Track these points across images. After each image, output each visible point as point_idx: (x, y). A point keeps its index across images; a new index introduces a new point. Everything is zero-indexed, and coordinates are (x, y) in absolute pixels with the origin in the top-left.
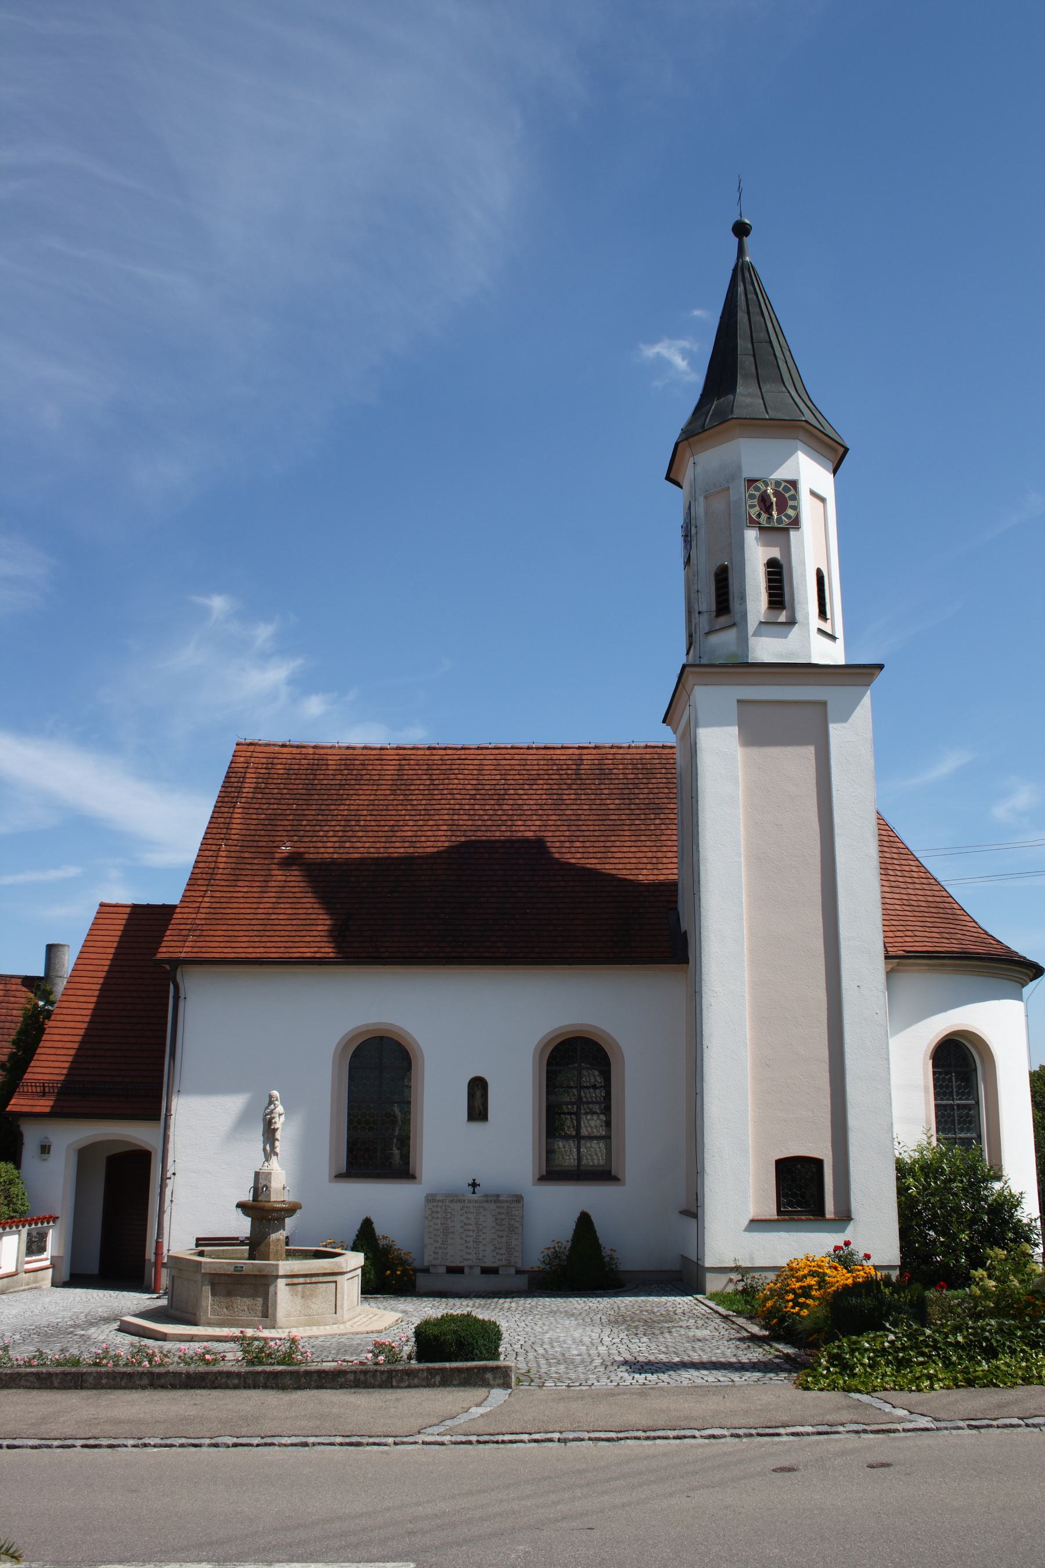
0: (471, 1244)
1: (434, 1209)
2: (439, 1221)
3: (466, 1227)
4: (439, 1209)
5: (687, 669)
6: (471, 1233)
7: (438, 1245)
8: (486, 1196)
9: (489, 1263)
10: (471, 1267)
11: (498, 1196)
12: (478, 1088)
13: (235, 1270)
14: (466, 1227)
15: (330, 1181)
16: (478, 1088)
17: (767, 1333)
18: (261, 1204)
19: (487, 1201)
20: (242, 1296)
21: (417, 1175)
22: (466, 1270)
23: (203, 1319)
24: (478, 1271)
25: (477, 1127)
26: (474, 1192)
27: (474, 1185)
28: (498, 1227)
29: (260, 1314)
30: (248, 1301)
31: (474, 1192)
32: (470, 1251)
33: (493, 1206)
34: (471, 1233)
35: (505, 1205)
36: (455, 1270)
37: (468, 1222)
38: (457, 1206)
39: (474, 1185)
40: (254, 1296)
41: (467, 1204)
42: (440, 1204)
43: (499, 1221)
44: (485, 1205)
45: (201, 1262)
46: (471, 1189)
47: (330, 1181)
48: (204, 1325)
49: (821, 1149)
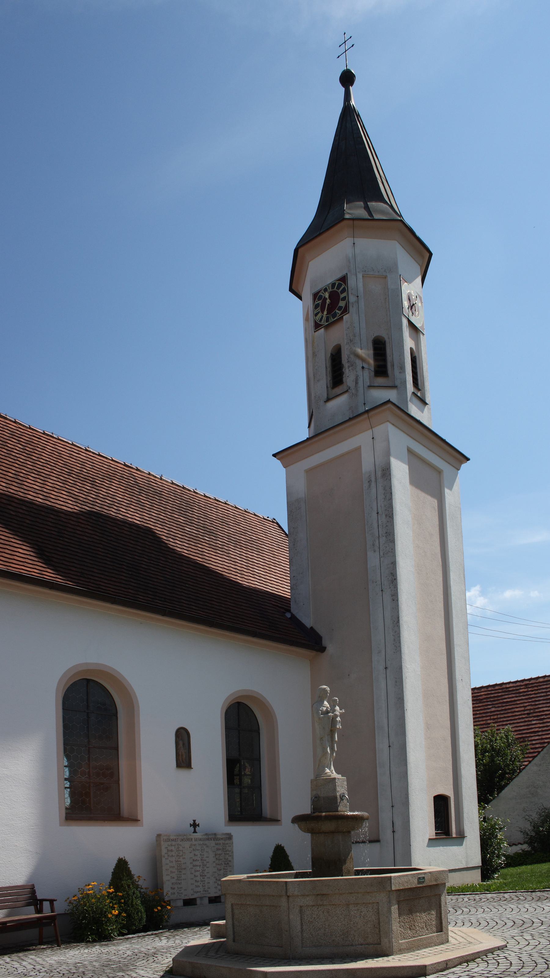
0: (198, 879)
1: (170, 848)
2: (173, 859)
3: (195, 863)
4: (173, 848)
5: (389, 405)
6: (198, 868)
7: (174, 881)
8: (206, 834)
9: (213, 895)
10: (201, 898)
11: (215, 834)
12: (183, 737)
13: (419, 883)
14: (195, 863)
15: (61, 825)
16: (183, 737)
17: (202, 937)
18: (340, 813)
19: (208, 839)
20: (420, 912)
21: (139, 818)
22: (198, 901)
23: (395, 948)
24: (206, 901)
25: (183, 773)
26: (195, 832)
27: (195, 825)
28: (217, 862)
29: (434, 929)
30: (424, 916)
31: (195, 832)
32: (199, 884)
33: (213, 843)
34: (198, 868)
35: (221, 842)
36: (189, 902)
37: (195, 858)
38: (187, 844)
39: (195, 825)
40: (427, 910)
41: (194, 842)
42: (174, 843)
43: (217, 856)
44: (207, 842)
45: (391, 877)
46: (192, 829)
47: (61, 825)
48: (397, 954)
49: (449, 792)
